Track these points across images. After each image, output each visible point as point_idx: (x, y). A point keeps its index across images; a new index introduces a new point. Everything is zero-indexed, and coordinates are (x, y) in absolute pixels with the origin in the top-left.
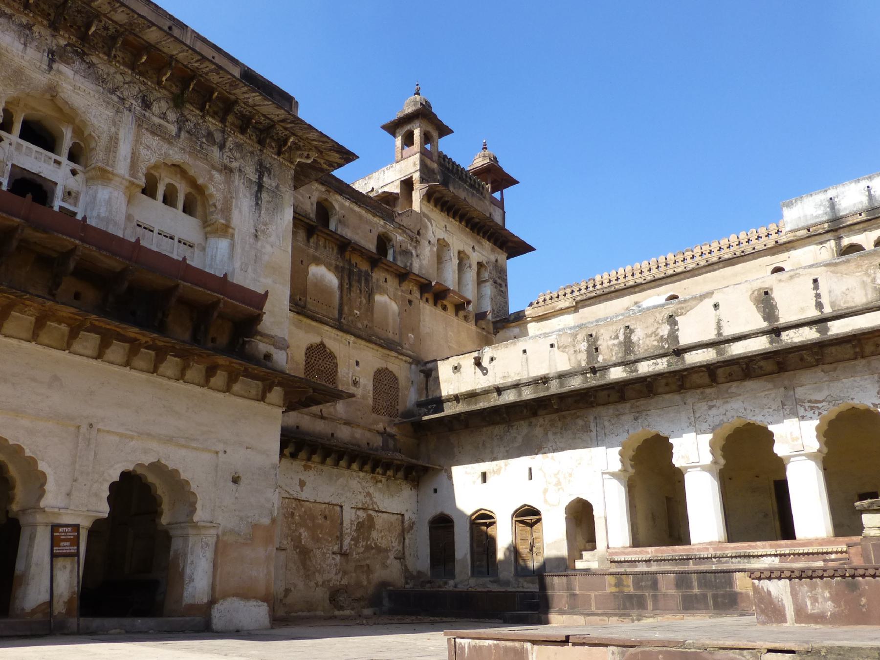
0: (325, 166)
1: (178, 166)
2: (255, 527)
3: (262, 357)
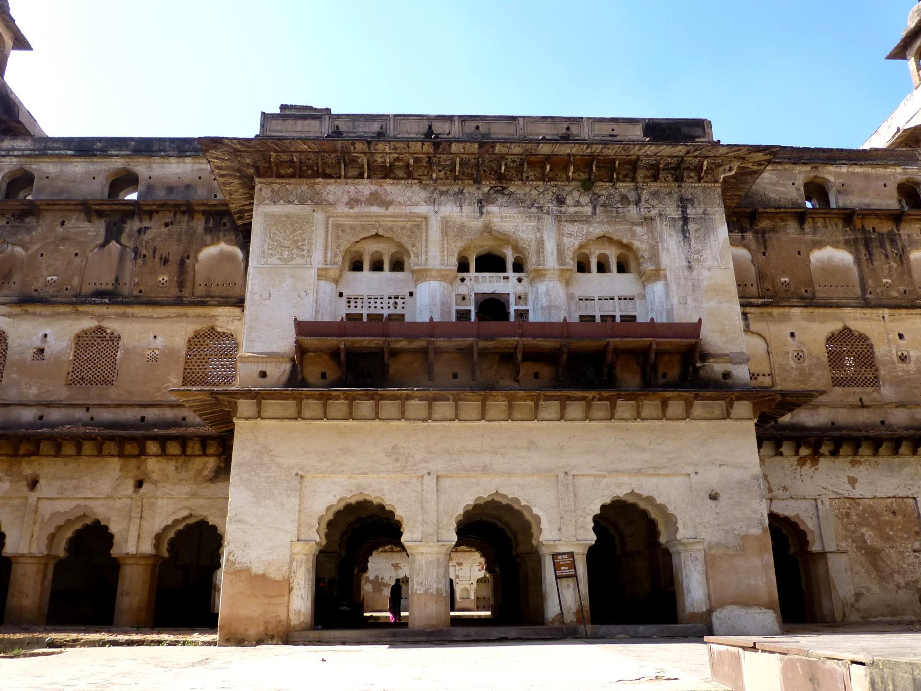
0: (755, 168)
1: (604, 236)
2: (745, 537)
3: (721, 377)
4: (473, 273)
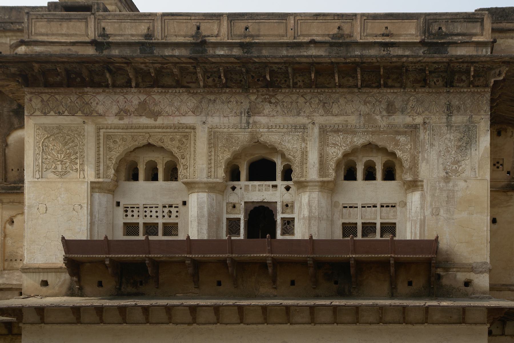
4: (243, 182)
